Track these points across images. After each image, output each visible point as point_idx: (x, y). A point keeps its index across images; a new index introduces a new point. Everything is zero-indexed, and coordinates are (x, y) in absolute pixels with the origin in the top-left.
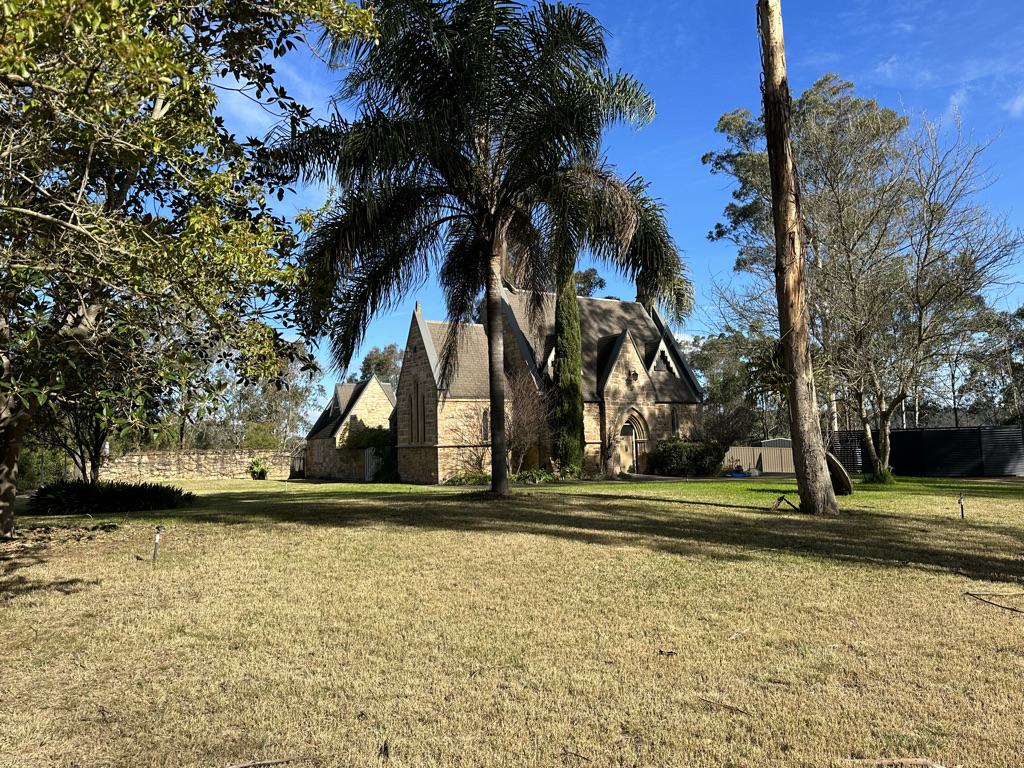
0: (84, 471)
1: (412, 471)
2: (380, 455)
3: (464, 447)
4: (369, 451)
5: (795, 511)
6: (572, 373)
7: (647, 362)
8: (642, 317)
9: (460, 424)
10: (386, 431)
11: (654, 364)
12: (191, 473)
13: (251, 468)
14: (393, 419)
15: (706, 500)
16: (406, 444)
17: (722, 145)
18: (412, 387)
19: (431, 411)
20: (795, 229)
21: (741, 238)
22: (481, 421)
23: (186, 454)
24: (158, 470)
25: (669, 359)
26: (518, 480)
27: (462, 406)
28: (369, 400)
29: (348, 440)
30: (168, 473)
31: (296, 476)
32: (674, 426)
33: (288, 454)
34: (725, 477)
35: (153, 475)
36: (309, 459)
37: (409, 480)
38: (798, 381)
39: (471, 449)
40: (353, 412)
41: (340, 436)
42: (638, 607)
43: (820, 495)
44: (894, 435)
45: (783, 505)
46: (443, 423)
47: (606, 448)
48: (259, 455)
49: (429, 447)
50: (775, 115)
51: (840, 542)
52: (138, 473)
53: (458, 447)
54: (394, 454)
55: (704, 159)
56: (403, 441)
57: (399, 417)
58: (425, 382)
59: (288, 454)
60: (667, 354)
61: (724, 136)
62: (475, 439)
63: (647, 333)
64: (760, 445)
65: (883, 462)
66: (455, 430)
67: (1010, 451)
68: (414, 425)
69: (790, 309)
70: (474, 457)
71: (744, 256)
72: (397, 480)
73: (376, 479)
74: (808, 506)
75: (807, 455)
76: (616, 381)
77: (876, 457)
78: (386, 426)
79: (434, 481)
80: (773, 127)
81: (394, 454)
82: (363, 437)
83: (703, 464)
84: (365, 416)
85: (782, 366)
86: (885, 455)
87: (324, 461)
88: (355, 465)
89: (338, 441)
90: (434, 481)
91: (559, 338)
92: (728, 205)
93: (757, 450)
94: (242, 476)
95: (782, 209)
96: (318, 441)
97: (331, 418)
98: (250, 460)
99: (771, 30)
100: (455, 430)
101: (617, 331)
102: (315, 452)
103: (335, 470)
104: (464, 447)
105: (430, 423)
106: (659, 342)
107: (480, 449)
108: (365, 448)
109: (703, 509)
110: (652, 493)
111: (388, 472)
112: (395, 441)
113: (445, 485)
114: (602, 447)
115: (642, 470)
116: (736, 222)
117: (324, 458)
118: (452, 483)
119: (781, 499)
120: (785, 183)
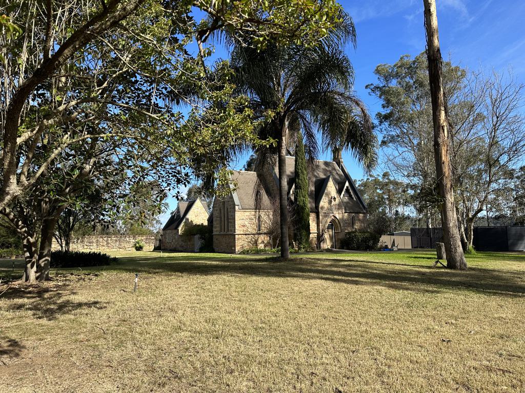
0: (62, 247)
1: (221, 246)
2: (203, 239)
3: (249, 234)
4: (197, 237)
5: (444, 267)
6: (304, 197)
7: (339, 192)
8: (334, 169)
9: (246, 223)
10: (205, 226)
11: (343, 193)
12: (104, 247)
13: (135, 245)
14: (210, 220)
15: (394, 262)
17: (377, 81)
19: (232, 216)
20: (444, 124)
21: (383, 129)
23: (101, 237)
24: (87, 245)
25: (351, 191)
26: (277, 251)
27: (247, 214)
28: (196, 211)
30: (91, 247)
31: (157, 249)
32: (353, 224)
33: (153, 238)
34: (380, 250)
35: (84, 248)
36: (164, 240)
37: (219, 251)
38: (447, 201)
40: (188, 216)
41: (181, 229)
43: (458, 259)
44: (476, 230)
45: (439, 265)
46: (238, 223)
47: (320, 238)
48: (139, 238)
50: (435, 66)
52: (76, 247)
53: (246, 234)
54: (213, 237)
55: (367, 87)
56: (216, 231)
59: (153, 238)
60: (349, 188)
61: (378, 76)
62: (254, 230)
63: (337, 177)
64: (393, 235)
65: (470, 243)
66: (244, 226)
67: (520, 238)
68: (223, 223)
69: (443, 165)
70: (253, 240)
71: (386, 139)
72: (213, 251)
73: (201, 251)
74: (452, 264)
75: (451, 239)
76: (324, 203)
77: (466, 241)
78: (206, 223)
79: (233, 252)
80: (433, 71)
81: (213, 237)
82: (194, 230)
83: (368, 243)
85: (438, 193)
86: (471, 240)
88: (189, 243)
89: (180, 231)
90: (233, 252)
91: (297, 180)
92: (377, 113)
93: (393, 237)
94: (129, 249)
95: (438, 114)
96: (168, 231)
97: (175, 220)
98: (134, 241)
99: (432, 23)
100: (244, 226)
101: (322, 176)
103: (178, 246)
104: (249, 234)
105: (231, 222)
106: (346, 182)
107: (256, 236)
108: (195, 235)
109: (397, 268)
110: (361, 259)
111: (208, 247)
112: (211, 231)
113: (240, 254)
114: (318, 235)
115: (338, 247)
116: (381, 122)
118: (243, 253)
119: (437, 262)
120: (439, 101)
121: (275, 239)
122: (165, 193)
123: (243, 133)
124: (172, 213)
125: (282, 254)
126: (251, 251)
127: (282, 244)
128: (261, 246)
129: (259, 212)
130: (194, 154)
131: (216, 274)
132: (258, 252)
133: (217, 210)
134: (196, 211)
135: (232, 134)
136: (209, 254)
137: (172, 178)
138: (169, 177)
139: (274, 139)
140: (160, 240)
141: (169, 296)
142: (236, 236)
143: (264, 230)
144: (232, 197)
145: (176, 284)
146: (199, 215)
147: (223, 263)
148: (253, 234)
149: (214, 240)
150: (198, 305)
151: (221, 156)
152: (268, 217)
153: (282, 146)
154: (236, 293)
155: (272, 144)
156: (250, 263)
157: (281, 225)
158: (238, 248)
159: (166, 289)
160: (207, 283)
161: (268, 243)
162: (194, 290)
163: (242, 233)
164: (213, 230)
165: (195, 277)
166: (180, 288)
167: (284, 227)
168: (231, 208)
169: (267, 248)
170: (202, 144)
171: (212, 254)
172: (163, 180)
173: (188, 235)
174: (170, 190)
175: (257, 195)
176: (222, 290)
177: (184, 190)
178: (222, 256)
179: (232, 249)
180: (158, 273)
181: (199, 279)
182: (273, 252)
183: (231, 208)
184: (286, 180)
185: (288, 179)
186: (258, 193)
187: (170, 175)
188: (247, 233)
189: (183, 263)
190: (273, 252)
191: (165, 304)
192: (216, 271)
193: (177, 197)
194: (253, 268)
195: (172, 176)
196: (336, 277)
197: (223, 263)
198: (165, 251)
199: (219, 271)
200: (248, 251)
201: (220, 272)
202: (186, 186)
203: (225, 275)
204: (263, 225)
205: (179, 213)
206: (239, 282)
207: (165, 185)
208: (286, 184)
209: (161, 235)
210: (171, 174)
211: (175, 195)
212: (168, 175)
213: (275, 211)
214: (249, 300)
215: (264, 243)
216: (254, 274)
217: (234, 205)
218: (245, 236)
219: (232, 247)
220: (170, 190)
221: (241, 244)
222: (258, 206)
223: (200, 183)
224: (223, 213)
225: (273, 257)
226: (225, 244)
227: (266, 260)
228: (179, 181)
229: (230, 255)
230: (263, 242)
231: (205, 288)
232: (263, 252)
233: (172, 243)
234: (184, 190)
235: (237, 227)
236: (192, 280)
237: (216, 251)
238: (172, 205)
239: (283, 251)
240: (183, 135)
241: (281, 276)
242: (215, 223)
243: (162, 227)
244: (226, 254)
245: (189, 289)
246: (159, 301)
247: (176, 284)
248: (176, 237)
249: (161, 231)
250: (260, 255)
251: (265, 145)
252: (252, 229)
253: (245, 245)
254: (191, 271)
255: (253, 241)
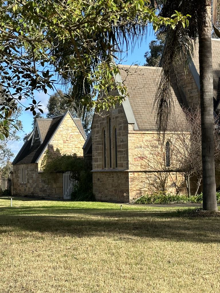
2: (77, 179)
4: (67, 174)
9: (146, 153)
10: (80, 158)
14: (88, 148)
16: (100, 169)
18: (105, 121)
19: (122, 141)
22: (164, 150)
27: (148, 137)
28: (64, 132)
29: (47, 166)
36: (15, 181)
37: (103, 199)
39: (156, 173)
40: (52, 142)
41: (41, 163)
42: (154, 284)
49: (121, 172)
51: (15, 214)
53: (145, 172)
54: (90, 176)
56: (97, 166)
57: (94, 147)
58: (117, 117)
66: (142, 158)
68: (107, 153)
70: (158, 180)
72: (93, 199)
73: (74, 198)
78: (80, 153)
79: (125, 200)
81: (90, 176)
82: (61, 165)
84: (62, 146)
87: (28, 182)
90: (125, 200)
96: (22, 166)
97: (32, 148)
100: (142, 158)
102: (20, 175)
103: (38, 190)
107: (163, 174)
111: (84, 192)
112: (89, 166)
113: (136, 203)
117: (28, 179)
118: (141, 202)
121: (194, 180)
122: (14, 104)
123: (133, 5)
124: (26, 138)
125: (205, 206)
126: (155, 200)
127: (205, 190)
128: (171, 191)
129: (164, 134)
130: (56, 41)
131: (96, 235)
132: (166, 201)
133: (98, 132)
134: (64, 132)
135: (115, 9)
136: (85, 202)
137: (23, 79)
138: (19, 78)
139: (184, 15)
140: (9, 180)
141: (23, 267)
142: (130, 175)
143: (175, 164)
144: (121, 110)
145: (34, 249)
146: (70, 139)
147: (107, 219)
148: (159, 171)
149: (95, 180)
150: (67, 284)
151: (101, 42)
152: (182, 144)
153: (205, 22)
154: (128, 266)
155: (180, 23)
156: (151, 219)
157: (204, 156)
158: (132, 195)
159: (17, 258)
160: (80, 250)
161: (184, 185)
162: (61, 259)
163: (139, 169)
164: (91, 165)
165: (63, 239)
166: (39, 256)
167: (208, 159)
168: (120, 129)
169: (181, 195)
170: (67, 26)
171: (91, 203)
172: (9, 84)
173: (52, 173)
174: (20, 98)
175: (161, 106)
176: (105, 261)
177: (43, 98)
178: (107, 207)
179: (123, 196)
180: (5, 231)
181: (67, 242)
182: (189, 202)
183: (120, 129)
184: (212, 81)
185: (217, 79)
186: (163, 103)
187: (21, 75)
188: (147, 170)
189: (45, 217)
190: (189, 202)
191: (16, 281)
192: (96, 230)
193: (32, 109)
194: (156, 227)
195: (23, 76)
196: (28, 209)
197: (107, 219)
198: (18, 197)
199: (100, 231)
200: (149, 199)
201: (103, 233)
202: (45, 91)
203: (109, 237)
204: (174, 157)
205: (38, 136)
206: (132, 249)
207: (12, 91)
208: (212, 87)
209: (11, 173)
210: (22, 72)
211: (30, 106)
212: (16, 75)
213: (194, 133)
214: (148, 278)
215: (175, 186)
216: (158, 236)
217: (126, 123)
218: (144, 175)
219: (122, 192)
220: (20, 98)
221: (138, 187)
222: (162, 127)
223: (67, 89)
224: (109, 135)
225: (190, 210)
226: (113, 187)
227: (178, 214)
228: (34, 84)
229: (119, 205)
230: (174, 185)
231: (78, 257)
232: (174, 200)
233: (29, 185)
234: (43, 98)
235: (130, 159)
236: (57, 244)
237: (97, 198)
238: (25, 125)
239: (206, 199)
240: (36, 13)
241: (201, 241)
242: (95, 153)
243: (12, 159)
244: (113, 204)
245: (53, 258)
246: (7, 275)
247: (34, 249)
248: (34, 175)
249: (11, 166)
250: (170, 205)
251: (169, 26)
252: (156, 162)
253: (145, 189)
254: (57, 230)
255: (157, 183)
